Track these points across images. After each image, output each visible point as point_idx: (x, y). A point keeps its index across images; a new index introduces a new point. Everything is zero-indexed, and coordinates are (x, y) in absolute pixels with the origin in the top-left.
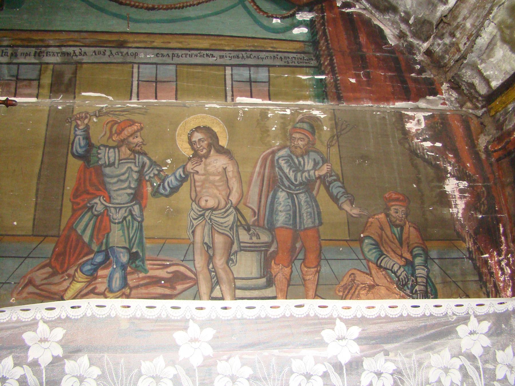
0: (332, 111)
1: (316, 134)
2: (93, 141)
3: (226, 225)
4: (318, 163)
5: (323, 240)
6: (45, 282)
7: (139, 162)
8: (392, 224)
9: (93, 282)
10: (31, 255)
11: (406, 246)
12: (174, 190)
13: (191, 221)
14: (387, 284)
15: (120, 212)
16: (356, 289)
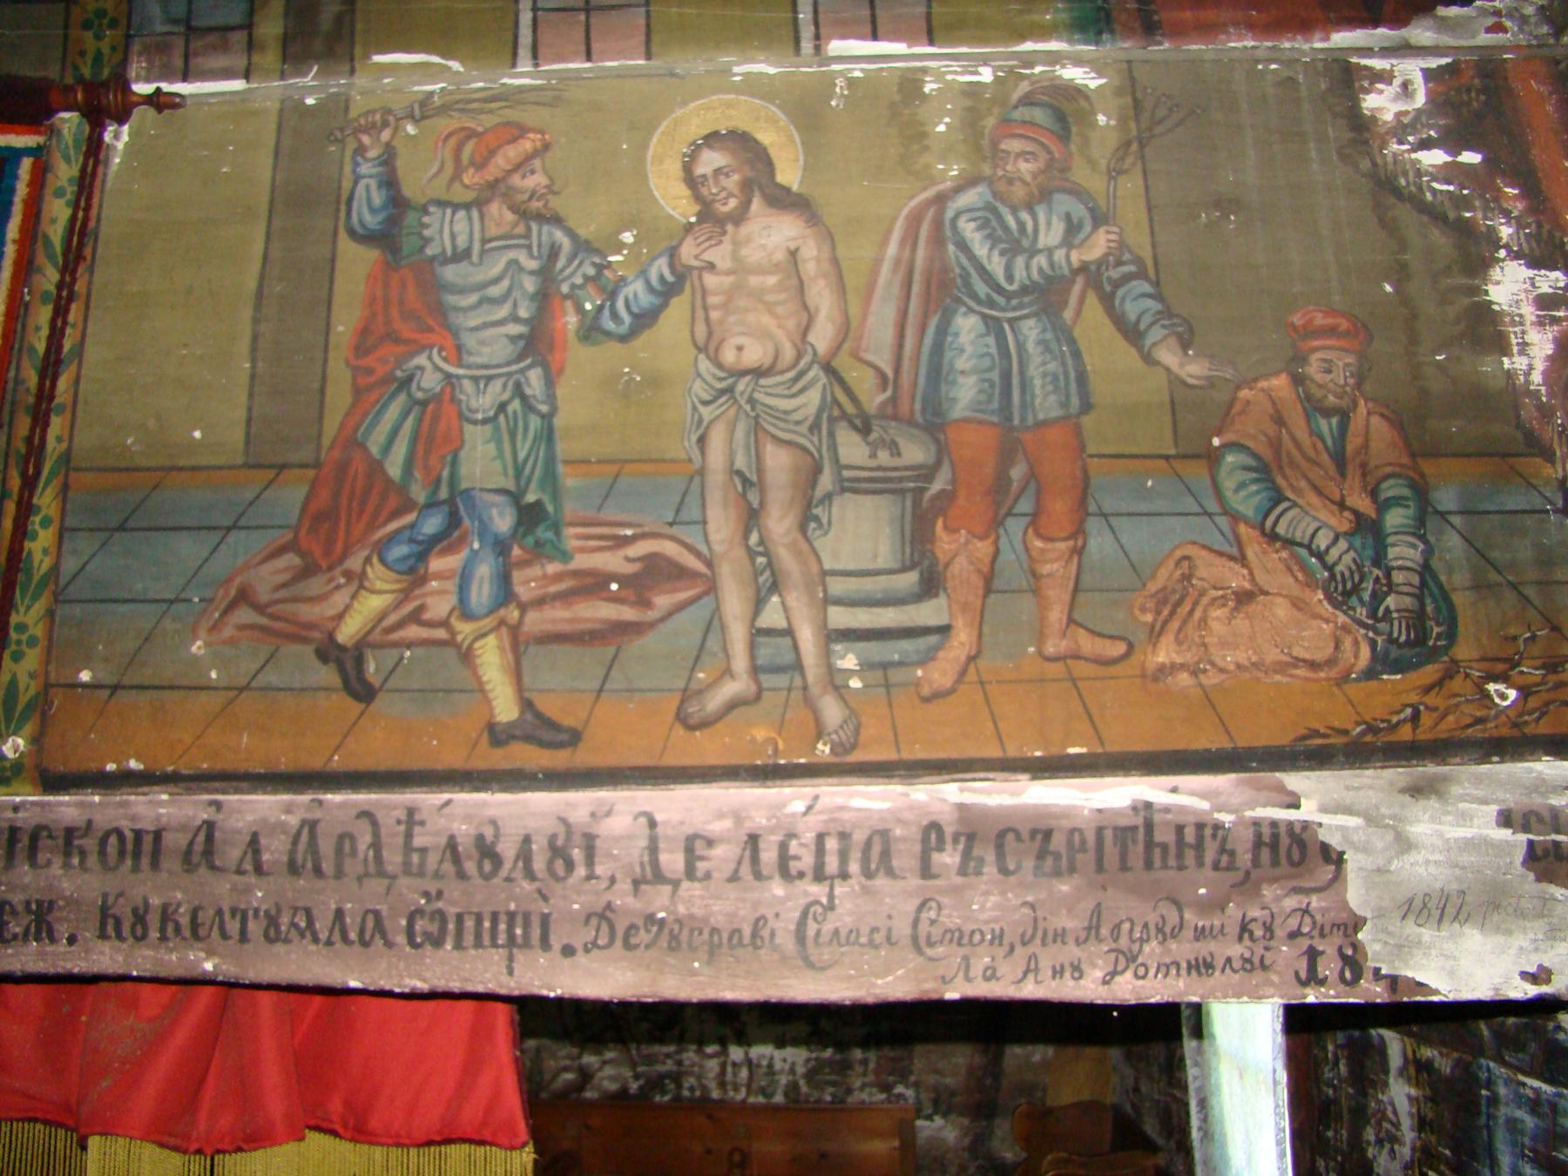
0: (1125, 66)
1: (1075, 138)
2: (409, 190)
3: (797, 417)
4: (1080, 227)
5: (1092, 456)
6: (278, 595)
7: (540, 245)
8: (1314, 407)
9: (417, 592)
10: (242, 522)
11: (1358, 473)
12: (645, 319)
13: (695, 409)
14: (1296, 591)
15: (490, 389)
16: (1195, 604)
